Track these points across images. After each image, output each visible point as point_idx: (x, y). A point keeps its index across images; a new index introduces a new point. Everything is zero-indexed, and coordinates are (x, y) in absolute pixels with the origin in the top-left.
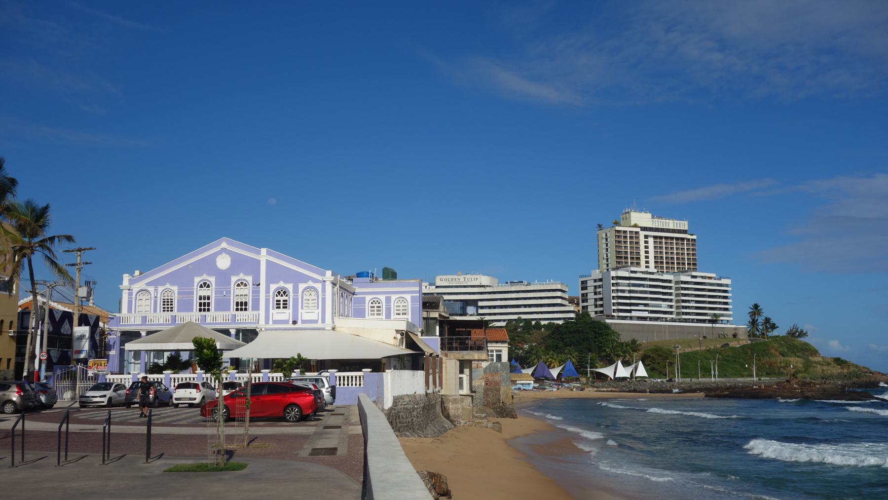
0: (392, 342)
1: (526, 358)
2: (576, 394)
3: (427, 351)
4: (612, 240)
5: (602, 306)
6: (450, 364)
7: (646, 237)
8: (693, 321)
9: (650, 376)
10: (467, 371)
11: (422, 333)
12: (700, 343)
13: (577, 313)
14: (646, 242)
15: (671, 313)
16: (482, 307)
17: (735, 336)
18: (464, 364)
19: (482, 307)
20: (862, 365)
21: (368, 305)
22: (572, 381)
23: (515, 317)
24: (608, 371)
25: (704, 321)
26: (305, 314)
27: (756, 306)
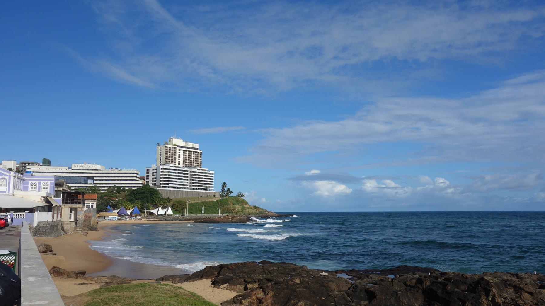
0: (40, 200)
1: (116, 205)
2: (137, 221)
3: (54, 204)
4: (164, 151)
5: (155, 181)
6: (66, 209)
7: (180, 150)
9: (174, 213)
10: (73, 212)
11: (54, 197)
13: (144, 184)
14: (179, 153)
15: (187, 185)
16: (96, 180)
17: (214, 196)
18: (72, 210)
19: (96, 180)
21: (30, 185)
22: (137, 216)
23: (113, 185)
24: (155, 211)
25: (201, 189)
27: (224, 183)
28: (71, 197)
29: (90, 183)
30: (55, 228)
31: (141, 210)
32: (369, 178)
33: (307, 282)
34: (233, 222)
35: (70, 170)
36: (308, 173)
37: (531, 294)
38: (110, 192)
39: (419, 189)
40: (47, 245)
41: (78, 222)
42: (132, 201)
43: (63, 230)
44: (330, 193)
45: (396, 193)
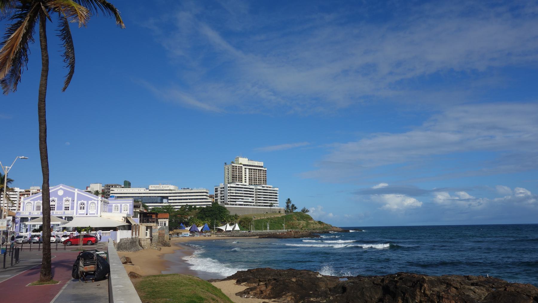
0: (121, 221)
1: (189, 222)
2: (207, 238)
3: (133, 223)
4: (230, 170)
5: (223, 199)
6: (143, 227)
7: (245, 169)
8: (262, 206)
9: (241, 229)
10: (149, 230)
12: (265, 216)
13: (213, 202)
15: (253, 202)
16: (170, 200)
17: (279, 212)
18: (147, 228)
19: (170, 200)
20: (329, 224)
22: (207, 232)
23: (185, 204)
24: (223, 228)
25: (267, 206)
26: (90, 212)
27: (289, 199)
28: (147, 217)
29: (165, 203)
30: (134, 244)
31: (211, 227)
32: (439, 190)
33: (302, 281)
34: (295, 238)
35: (148, 191)
36: (375, 187)
37: (456, 288)
38: (183, 211)
39: (496, 200)
40: (127, 258)
41: (153, 239)
42: (202, 219)
43: (141, 246)
44: (399, 206)
45: (470, 205)
